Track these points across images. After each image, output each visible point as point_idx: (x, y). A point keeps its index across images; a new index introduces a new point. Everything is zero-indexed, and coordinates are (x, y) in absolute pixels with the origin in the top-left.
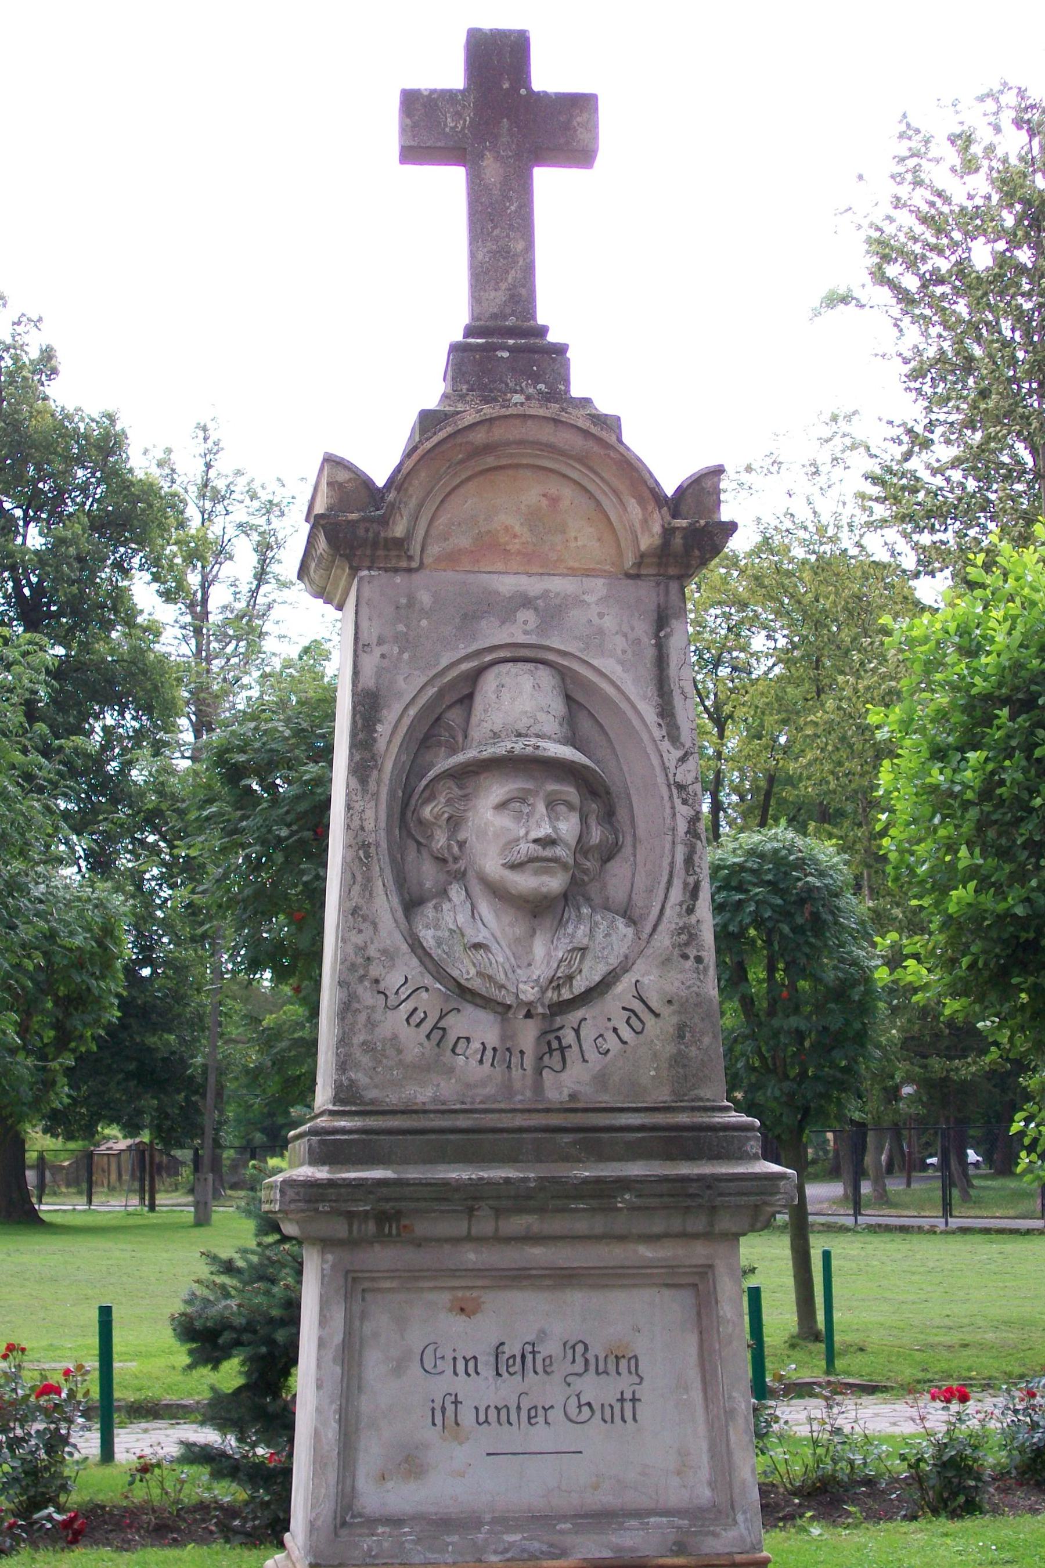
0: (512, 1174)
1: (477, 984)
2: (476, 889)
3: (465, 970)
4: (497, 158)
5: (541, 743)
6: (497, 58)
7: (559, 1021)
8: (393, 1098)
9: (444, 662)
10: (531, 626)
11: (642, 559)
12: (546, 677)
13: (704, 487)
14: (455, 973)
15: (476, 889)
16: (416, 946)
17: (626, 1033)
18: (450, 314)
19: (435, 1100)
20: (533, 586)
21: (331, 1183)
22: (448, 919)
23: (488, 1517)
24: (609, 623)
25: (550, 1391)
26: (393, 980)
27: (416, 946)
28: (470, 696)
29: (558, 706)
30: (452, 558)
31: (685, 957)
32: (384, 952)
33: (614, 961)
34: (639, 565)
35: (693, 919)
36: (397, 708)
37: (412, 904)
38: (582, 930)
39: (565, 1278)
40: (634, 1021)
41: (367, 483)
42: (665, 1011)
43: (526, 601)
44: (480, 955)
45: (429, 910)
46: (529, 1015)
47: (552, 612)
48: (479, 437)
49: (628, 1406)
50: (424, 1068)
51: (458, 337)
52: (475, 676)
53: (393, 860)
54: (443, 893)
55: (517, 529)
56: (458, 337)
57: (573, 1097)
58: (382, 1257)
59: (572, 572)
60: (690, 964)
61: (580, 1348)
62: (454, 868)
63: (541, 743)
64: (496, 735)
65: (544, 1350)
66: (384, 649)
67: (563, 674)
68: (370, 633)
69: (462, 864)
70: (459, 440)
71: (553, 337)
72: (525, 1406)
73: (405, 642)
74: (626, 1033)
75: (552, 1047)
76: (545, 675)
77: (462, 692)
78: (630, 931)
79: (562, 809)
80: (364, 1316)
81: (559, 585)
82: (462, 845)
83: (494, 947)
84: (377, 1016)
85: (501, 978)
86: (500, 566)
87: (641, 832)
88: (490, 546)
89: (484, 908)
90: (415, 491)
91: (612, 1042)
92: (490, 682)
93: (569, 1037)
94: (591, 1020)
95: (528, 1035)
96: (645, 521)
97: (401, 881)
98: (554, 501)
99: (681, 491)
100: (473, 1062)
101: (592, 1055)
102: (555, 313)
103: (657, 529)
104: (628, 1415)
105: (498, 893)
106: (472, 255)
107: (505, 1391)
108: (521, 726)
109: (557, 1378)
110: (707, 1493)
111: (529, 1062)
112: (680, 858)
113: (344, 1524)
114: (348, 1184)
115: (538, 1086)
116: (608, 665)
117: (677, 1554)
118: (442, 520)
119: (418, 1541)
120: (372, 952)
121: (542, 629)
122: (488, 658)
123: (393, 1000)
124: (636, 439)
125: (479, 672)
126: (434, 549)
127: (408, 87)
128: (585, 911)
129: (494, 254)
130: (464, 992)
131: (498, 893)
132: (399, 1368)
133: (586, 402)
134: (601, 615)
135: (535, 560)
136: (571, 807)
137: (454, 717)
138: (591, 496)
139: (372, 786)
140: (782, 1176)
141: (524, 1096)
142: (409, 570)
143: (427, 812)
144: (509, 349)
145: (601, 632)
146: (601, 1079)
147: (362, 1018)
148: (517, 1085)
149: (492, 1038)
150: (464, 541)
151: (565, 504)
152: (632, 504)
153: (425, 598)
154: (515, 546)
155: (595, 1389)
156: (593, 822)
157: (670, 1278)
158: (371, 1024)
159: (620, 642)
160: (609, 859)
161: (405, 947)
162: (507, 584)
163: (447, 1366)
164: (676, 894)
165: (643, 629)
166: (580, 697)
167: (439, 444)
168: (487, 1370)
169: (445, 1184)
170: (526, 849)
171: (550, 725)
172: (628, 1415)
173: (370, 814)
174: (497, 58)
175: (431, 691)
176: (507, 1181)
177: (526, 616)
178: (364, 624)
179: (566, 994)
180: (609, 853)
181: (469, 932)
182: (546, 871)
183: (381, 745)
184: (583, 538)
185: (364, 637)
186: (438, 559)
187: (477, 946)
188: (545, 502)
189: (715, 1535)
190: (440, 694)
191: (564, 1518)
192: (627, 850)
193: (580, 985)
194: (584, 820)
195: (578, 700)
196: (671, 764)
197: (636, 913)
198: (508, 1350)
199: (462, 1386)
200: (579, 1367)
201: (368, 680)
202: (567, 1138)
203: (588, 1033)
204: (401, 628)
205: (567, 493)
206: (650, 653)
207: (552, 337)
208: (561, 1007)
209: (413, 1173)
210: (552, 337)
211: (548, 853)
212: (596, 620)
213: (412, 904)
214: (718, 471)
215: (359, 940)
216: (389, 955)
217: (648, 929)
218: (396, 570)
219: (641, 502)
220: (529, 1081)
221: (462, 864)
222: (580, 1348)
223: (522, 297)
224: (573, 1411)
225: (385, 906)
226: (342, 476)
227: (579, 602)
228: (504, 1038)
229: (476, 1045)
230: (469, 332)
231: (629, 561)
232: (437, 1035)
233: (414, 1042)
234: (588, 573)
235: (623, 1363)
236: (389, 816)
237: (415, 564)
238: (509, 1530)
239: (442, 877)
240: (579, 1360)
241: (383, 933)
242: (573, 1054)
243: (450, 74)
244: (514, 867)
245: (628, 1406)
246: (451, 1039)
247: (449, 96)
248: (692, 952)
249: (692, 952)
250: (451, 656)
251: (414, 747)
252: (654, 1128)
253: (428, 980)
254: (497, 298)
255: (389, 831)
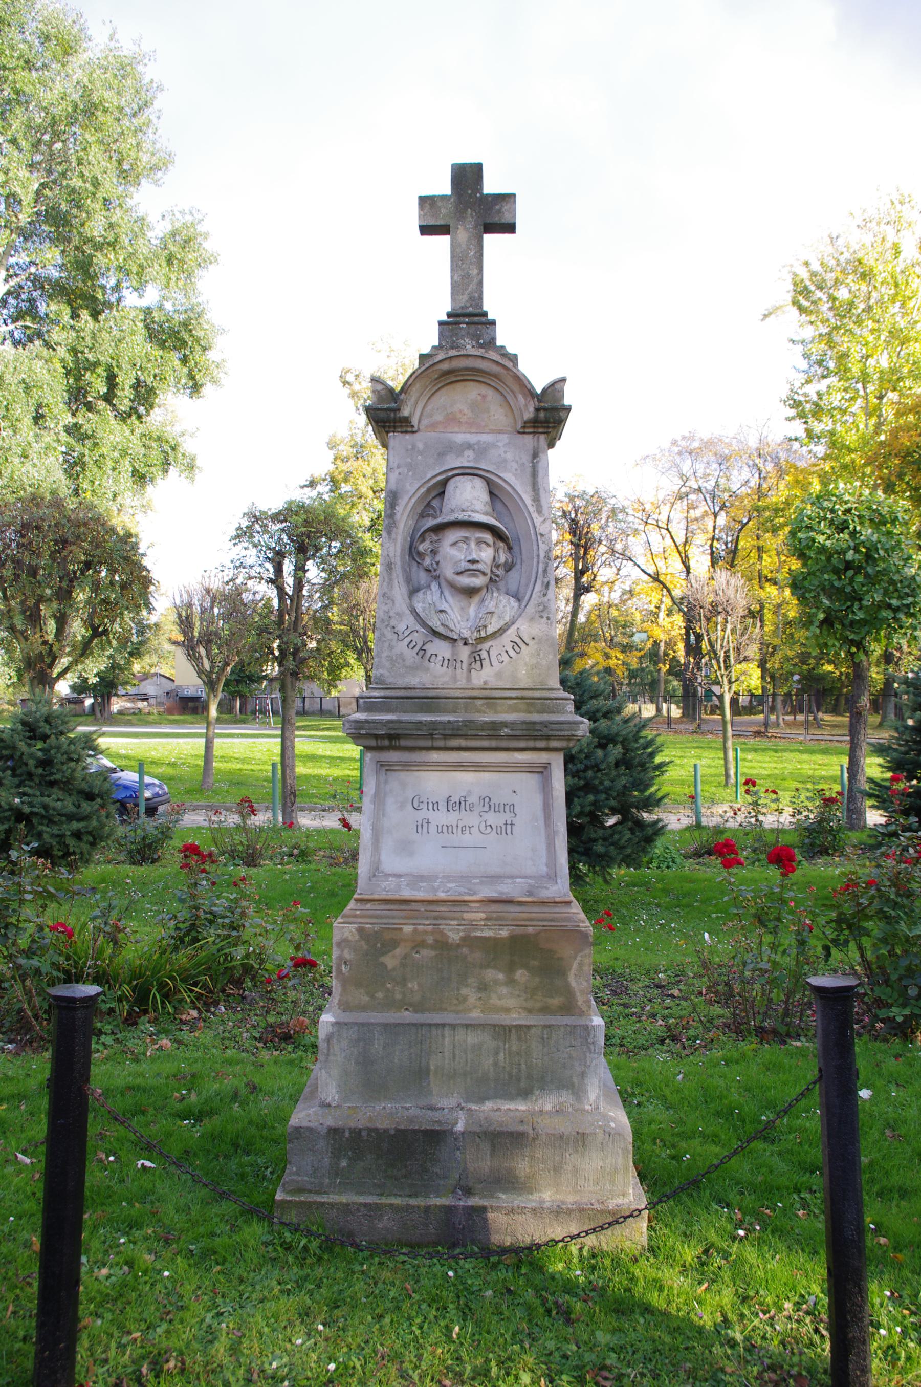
0: (452, 718)
1: (441, 630)
2: (444, 584)
3: (435, 623)
4: (466, 229)
5: (473, 515)
6: (467, 177)
7: (479, 647)
8: (401, 683)
9: (429, 476)
10: (471, 458)
11: (525, 424)
12: (479, 483)
13: (556, 387)
14: (430, 624)
15: (444, 584)
16: (414, 612)
17: (512, 653)
18: (442, 306)
19: (420, 683)
20: (472, 438)
21: (367, 721)
22: (429, 598)
23: (441, 875)
24: (509, 456)
25: (471, 819)
26: (401, 627)
27: (414, 612)
28: (443, 493)
29: (485, 497)
30: (433, 426)
31: (542, 617)
32: (397, 614)
33: (507, 619)
34: (524, 427)
35: (546, 599)
36: (406, 498)
37: (413, 591)
38: (493, 603)
39: (460, 767)
40: (516, 647)
41: (391, 390)
42: (531, 643)
43: (469, 446)
44: (442, 616)
45: (420, 594)
46: (465, 644)
47: (481, 451)
48: (445, 366)
49: (509, 827)
50: (414, 669)
51: (444, 318)
52: (444, 483)
53: (404, 571)
54: (429, 586)
55: (466, 411)
56: (444, 318)
57: (485, 683)
58: (393, 756)
59: (492, 432)
60: (545, 619)
61: (487, 800)
62: (433, 573)
63: (473, 515)
64: (452, 511)
65: (470, 800)
66: (400, 470)
67: (488, 482)
68: (394, 462)
69: (438, 573)
70: (436, 367)
71: (490, 317)
72: (460, 825)
73: (411, 467)
74: (512, 653)
75: (476, 659)
76: (478, 482)
77: (440, 489)
78: (516, 605)
79: (484, 546)
80: (386, 782)
81: (485, 438)
82: (438, 563)
83: (449, 611)
84: (394, 643)
85: (452, 626)
86: (456, 429)
87: (524, 557)
88: (452, 419)
89: (447, 593)
90: (414, 392)
91: (505, 657)
92: (451, 483)
93: (484, 654)
94: (496, 647)
95: (464, 653)
96: (526, 406)
97: (408, 580)
98: (484, 397)
99: (544, 391)
100: (438, 666)
101: (495, 662)
102: (491, 306)
103: (532, 409)
104: (509, 831)
105: (452, 586)
106: (452, 278)
107: (451, 818)
108: (464, 507)
109: (476, 813)
110: (545, 869)
111: (465, 666)
112: (541, 570)
113: (374, 876)
114: (374, 722)
115: (469, 679)
116: (508, 476)
117: (528, 896)
118: (429, 408)
119: (408, 885)
120: (391, 614)
121: (476, 460)
122: (450, 474)
123: (401, 637)
124: (525, 367)
125: (447, 480)
126: (425, 422)
127: (423, 194)
128: (495, 595)
129: (463, 277)
130: (435, 633)
131: (452, 586)
132: (402, 807)
133: (503, 347)
134: (505, 452)
135: (474, 426)
136: (488, 545)
137: (435, 503)
138: (502, 394)
139: (393, 535)
140: (582, 723)
141: (462, 683)
142: (413, 432)
143: (421, 548)
144: (467, 323)
145: (505, 460)
146: (499, 675)
147: (386, 644)
148: (459, 677)
149: (448, 655)
150: (439, 417)
151: (489, 398)
152: (520, 398)
153: (420, 446)
154: (464, 419)
155: (494, 819)
156: (501, 552)
157: (530, 769)
158: (391, 648)
159: (515, 465)
160: (510, 570)
161: (408, 612)
162: (460, 438)
163: (424, 806)
164: (538, 587)
165: (526, 458)
166: (496, 492)
167: (436, 372)
168: (443, 808)
169: (420, 722)
170: (464, 565)
171: (479, 506)
172: (509, 831)
173: (392, 549)
174: (467, 177)
175: (423, 490)
176: (449, 722)
177: (469, 453)
178: (391, 459)
179: (483, 634)
180: (509, 567)
181: (438, 604)
182: (474, 576)
183: (398, 516)
184: (498, 415)
185: (391, 463)
186: (426, 427)
187: (441, 611)
188: (479, 398)
189: (546, 888)
190: (429, 490)
191: (476, 877)
192: (518, 566)
193: (491, 630)
194: (497, 550)
195: (494, 493)
196: (537, 524)
197: (520, 596)
198: (453, 800)
199: (431, 815)
200: (486, 808)
201: (393, 486)
202: (479, 702)
203: (493, 653)
204: (409, 460)
205: (490, 393)
206: (529, 470)
207: (490, 317)
208: (481, 640)
209: (406, 717)
210: (490, 317)
211: (474, 567)
212: (503, 455)
213: (413, 591)
214: (563, 380)
215: (386, 608)
216: (400, 615)
217: (524, 604)
218: (406, 432)
219: (524, 396)
220: (465, 675)
221: (438, 573)
222: (487, 800)
223: (477, 298)
224: (482, 828)
225: (399, 592)
226: (379, 387)
227: (494, 446)
228: (453, 654)
229: (440, 658)
230: (449, 315)
231: (519, 425)
232: (421, 653)
233: (410, 655)
234: (500, 432)
235: (507, 808)
236: (402, 550)
237: (416, 429)
238: (449, 882)
239: (429, 579)
240: (487, 806)
241: (397, 605)
242: (486, 663)
243: (444, 187)
244: (459, 574)
245: (509, 827)
246: (428, 655)
247: (443, 198)
248: (545, 615)
249: (545, 615)
250: (432, 472)
251: (416, 517)
252: (522, 698)
253: (418, 627)
254: (464, 299)
255: (402, 557)
